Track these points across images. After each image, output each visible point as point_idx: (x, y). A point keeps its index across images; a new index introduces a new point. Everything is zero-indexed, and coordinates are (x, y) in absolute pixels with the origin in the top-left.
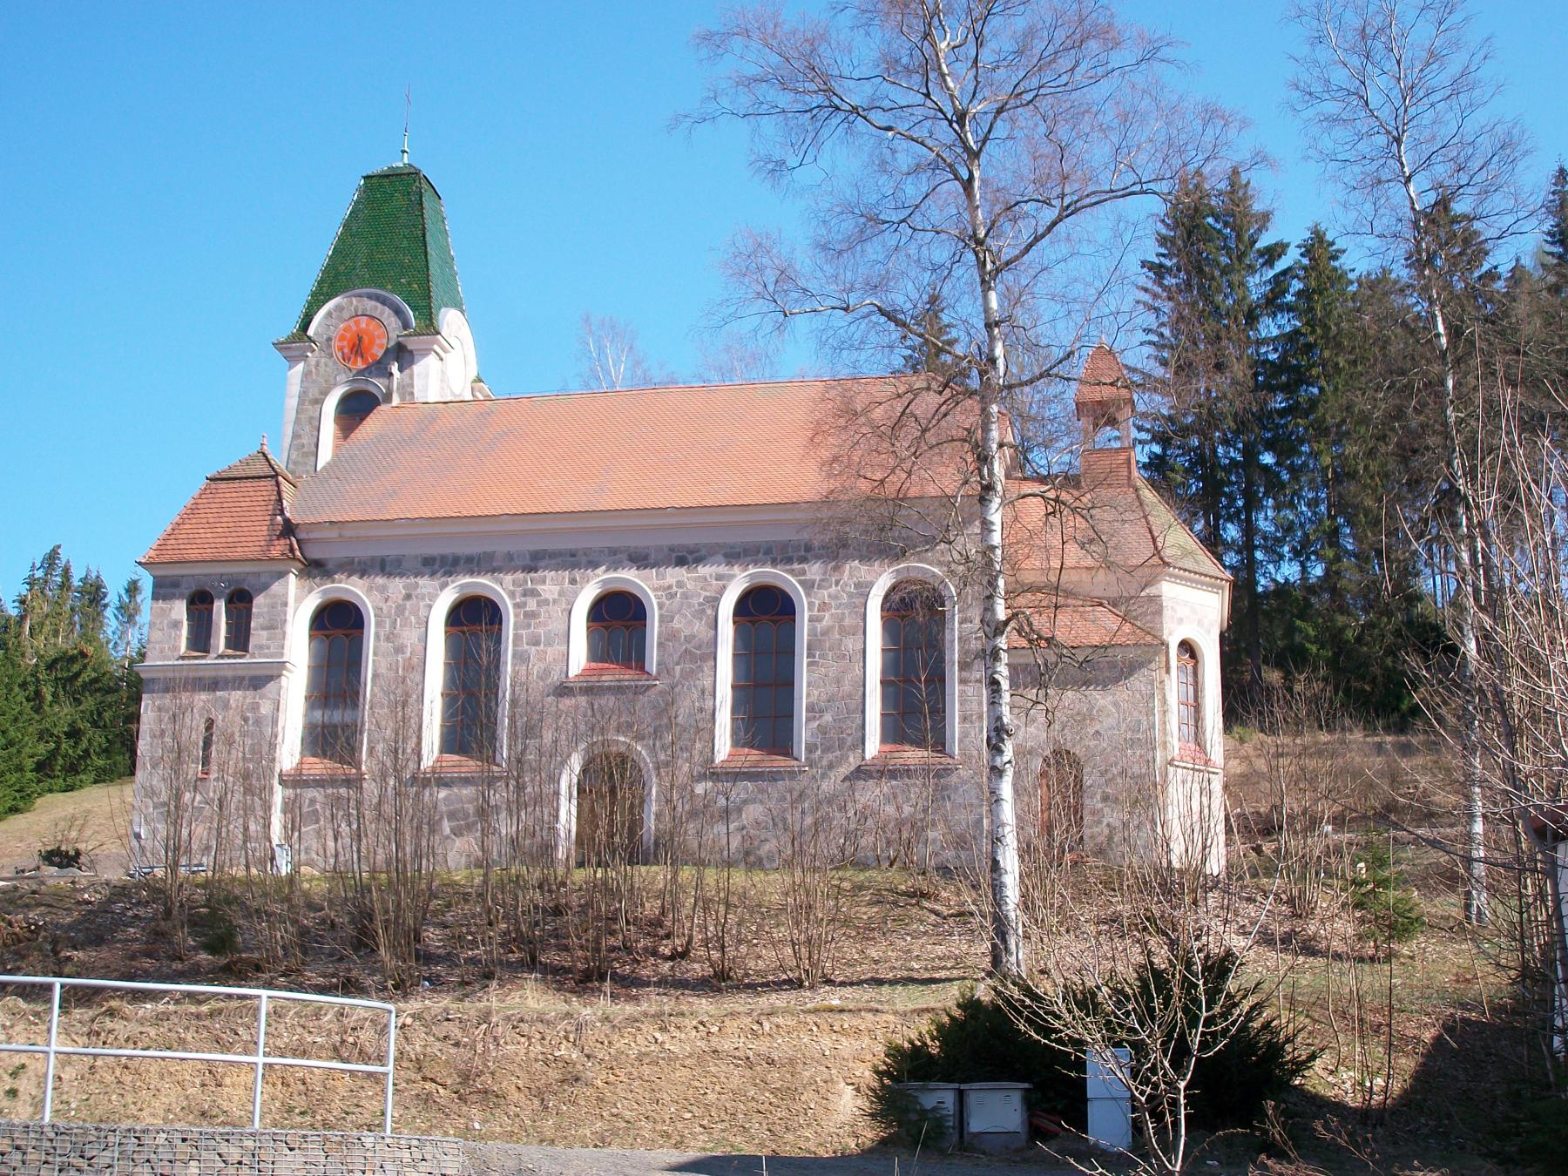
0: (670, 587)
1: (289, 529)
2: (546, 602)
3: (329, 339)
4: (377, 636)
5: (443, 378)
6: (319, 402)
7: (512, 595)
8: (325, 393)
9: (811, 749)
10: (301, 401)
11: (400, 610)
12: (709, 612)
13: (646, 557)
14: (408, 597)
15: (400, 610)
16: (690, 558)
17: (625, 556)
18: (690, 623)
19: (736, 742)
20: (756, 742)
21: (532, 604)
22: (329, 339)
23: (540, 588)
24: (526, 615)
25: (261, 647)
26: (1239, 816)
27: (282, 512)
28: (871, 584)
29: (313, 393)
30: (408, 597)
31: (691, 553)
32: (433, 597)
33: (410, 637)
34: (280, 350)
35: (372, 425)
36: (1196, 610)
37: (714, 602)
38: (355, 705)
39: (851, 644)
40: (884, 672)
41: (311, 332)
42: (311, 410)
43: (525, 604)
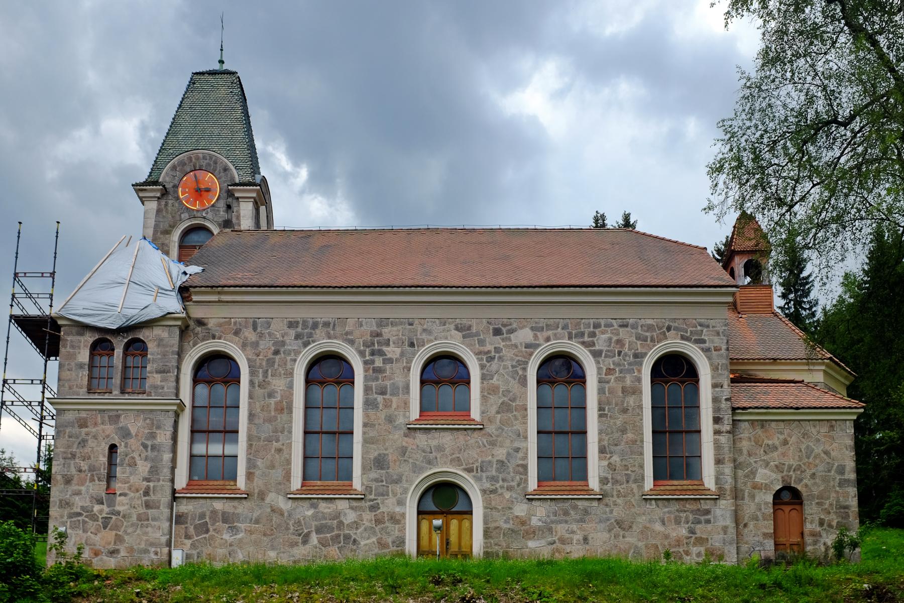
0: (489, 352)
2: (390, 361)
7: (362, 354)
8: (173, 226)
12: (520, 373)
14: (276, 352)
15: (271, 363)
16: (504, 330)
21: (379, 362)
23: (385, 349)
24: (375, 370)
25: (155, 387)
26: (572, 539)
29: (164, 226)
30: (276, 352)
31: (505, 325)
32: (297, 353)
33: (278, 384)
34: (137, 191)
35: (24, 348)
37: (524, 365)
39: (631, 401)
40: (698, 414)
43: (373, 362)
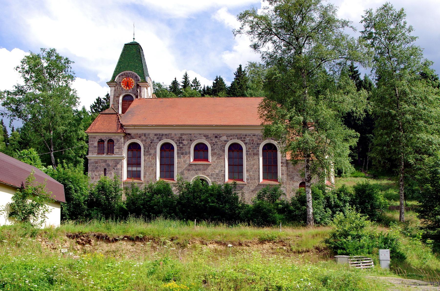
1: (122, 126)
2: (185, 145)
3: (120, 82)
4: (144, 151)
5: (148, 93)
6: (118, 97)
7: (176, 143)
8: (120, 95)
9: (247, 179)
10: (114, 97)
11: (150, 145)
13: (208, 136)
14: (151, 143)
15: (150, 145)
17: (203, 136)
18: (219, 151)
19: (229, 179)
20: (240, 178)
21: (181, 145)
22: (120, 82)
25: (117, 153)
27: (120, 122)
28: (260, 144)
29: (117, 95)
30: (151, 143)
36: (30, 239)
38: (140, 167)
41: (115, 80)
42: (117, 99)
43: (180, 145)
